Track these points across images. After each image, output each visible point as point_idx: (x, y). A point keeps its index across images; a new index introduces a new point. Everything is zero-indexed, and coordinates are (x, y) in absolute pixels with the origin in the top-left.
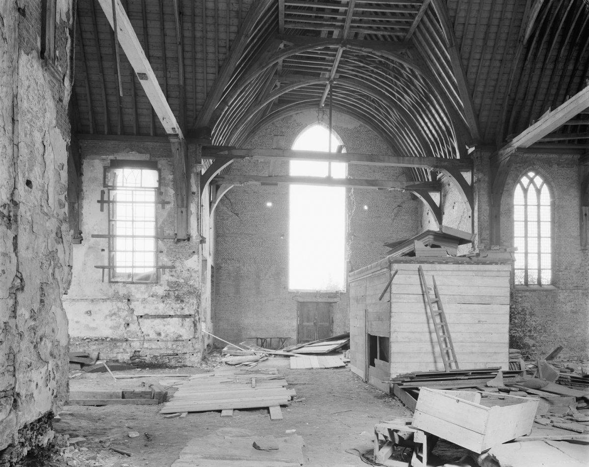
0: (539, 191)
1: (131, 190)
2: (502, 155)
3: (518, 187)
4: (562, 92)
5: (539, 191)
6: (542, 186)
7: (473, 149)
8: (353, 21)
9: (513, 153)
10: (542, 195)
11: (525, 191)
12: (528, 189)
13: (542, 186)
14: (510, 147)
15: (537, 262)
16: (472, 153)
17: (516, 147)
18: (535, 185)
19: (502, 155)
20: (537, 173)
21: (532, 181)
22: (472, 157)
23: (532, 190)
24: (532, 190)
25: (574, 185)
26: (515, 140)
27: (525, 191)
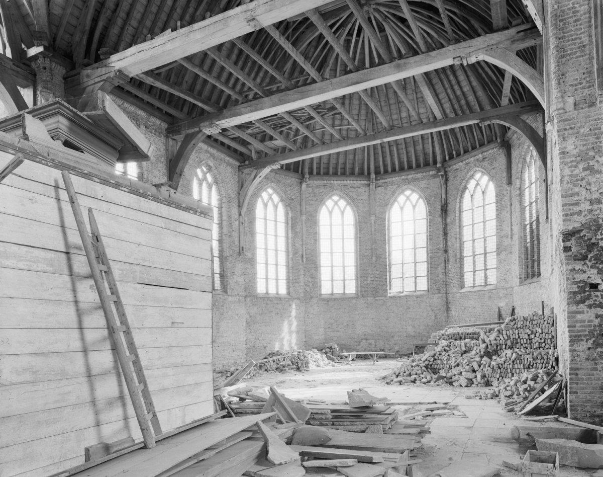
0: (276, 207)
1: (121, 392)
2: (88, 76)
3: (260, 200)
4: (160, 24)
5: (276, 207)
6: (345, 208)
7: (40, 49)
8: (236, 63)
9: (109, 77)
10: (268, 210)
11: (266, 205)
12: (344, 210)
13: (345, 208)
14: (106, 66)
15: (424, 206)
16: (35, 57)
17: (117, 68)
18: (339, 208)
19: (88, 76)
20: (341, 197)
21: (336, 203)
22: (33, 65)
23: (270, 206)
24: (270, 206)
25: (162, 160)
26: (114, 58)
27: (266, 205)
